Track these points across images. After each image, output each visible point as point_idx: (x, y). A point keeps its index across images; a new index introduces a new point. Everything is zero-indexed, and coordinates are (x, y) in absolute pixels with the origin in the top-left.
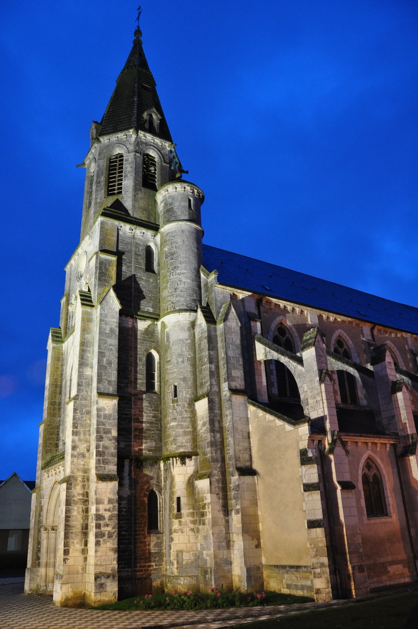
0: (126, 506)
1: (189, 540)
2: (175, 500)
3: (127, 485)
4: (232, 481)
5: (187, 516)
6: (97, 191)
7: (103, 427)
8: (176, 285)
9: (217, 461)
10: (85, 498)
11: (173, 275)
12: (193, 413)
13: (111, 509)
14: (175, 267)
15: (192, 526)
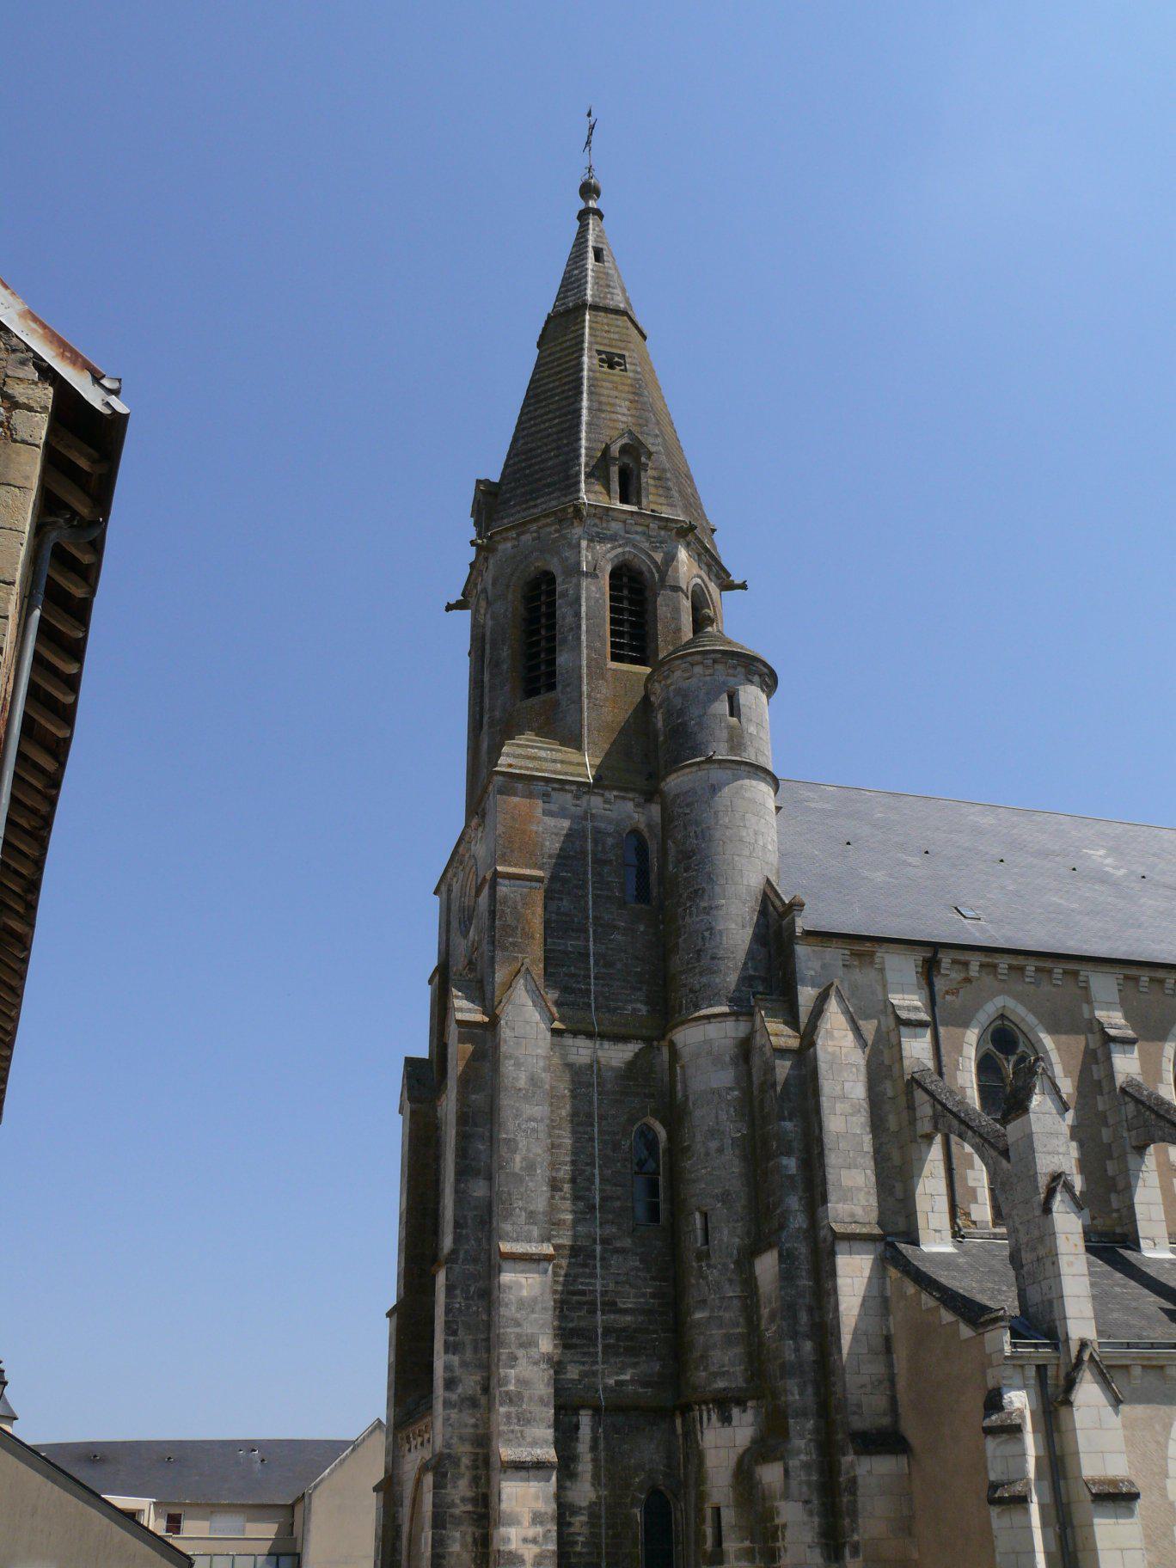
0: (585, 1530)
2: (709, 1513)
3: (588, 1476)
5: (737, 1558)
6: (492, 688)
7: (517, 1330)
8: (700, 942)
9: (805, 1415)
10: (481, 1510)
12: (749, 1283)
13: (540, 1539)
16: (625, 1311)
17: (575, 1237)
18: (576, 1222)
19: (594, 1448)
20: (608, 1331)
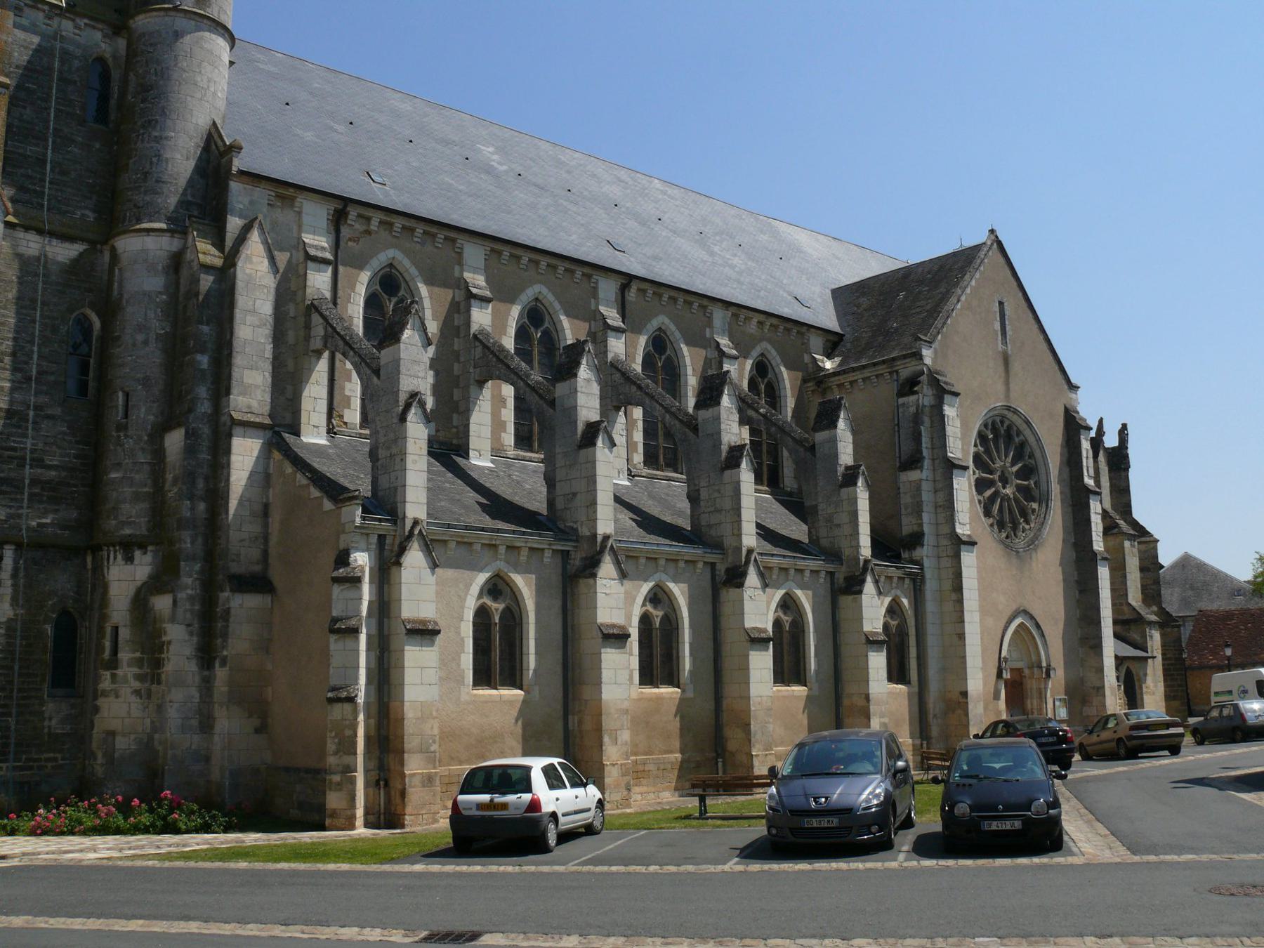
1: (129, 712)
2: (108, 630)
4: (221, 601)
5: (129, 666)
8: (148, 166)
11: (143, 141)
12: (159, 454)
14: (150, 121)
15: (137, 685)
16: (50, 467)
17: (11, 402)
18: (13, 390)
19: (14, 576)
20: (34, 482)
